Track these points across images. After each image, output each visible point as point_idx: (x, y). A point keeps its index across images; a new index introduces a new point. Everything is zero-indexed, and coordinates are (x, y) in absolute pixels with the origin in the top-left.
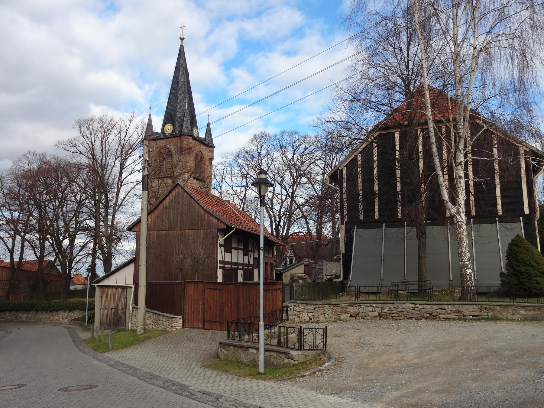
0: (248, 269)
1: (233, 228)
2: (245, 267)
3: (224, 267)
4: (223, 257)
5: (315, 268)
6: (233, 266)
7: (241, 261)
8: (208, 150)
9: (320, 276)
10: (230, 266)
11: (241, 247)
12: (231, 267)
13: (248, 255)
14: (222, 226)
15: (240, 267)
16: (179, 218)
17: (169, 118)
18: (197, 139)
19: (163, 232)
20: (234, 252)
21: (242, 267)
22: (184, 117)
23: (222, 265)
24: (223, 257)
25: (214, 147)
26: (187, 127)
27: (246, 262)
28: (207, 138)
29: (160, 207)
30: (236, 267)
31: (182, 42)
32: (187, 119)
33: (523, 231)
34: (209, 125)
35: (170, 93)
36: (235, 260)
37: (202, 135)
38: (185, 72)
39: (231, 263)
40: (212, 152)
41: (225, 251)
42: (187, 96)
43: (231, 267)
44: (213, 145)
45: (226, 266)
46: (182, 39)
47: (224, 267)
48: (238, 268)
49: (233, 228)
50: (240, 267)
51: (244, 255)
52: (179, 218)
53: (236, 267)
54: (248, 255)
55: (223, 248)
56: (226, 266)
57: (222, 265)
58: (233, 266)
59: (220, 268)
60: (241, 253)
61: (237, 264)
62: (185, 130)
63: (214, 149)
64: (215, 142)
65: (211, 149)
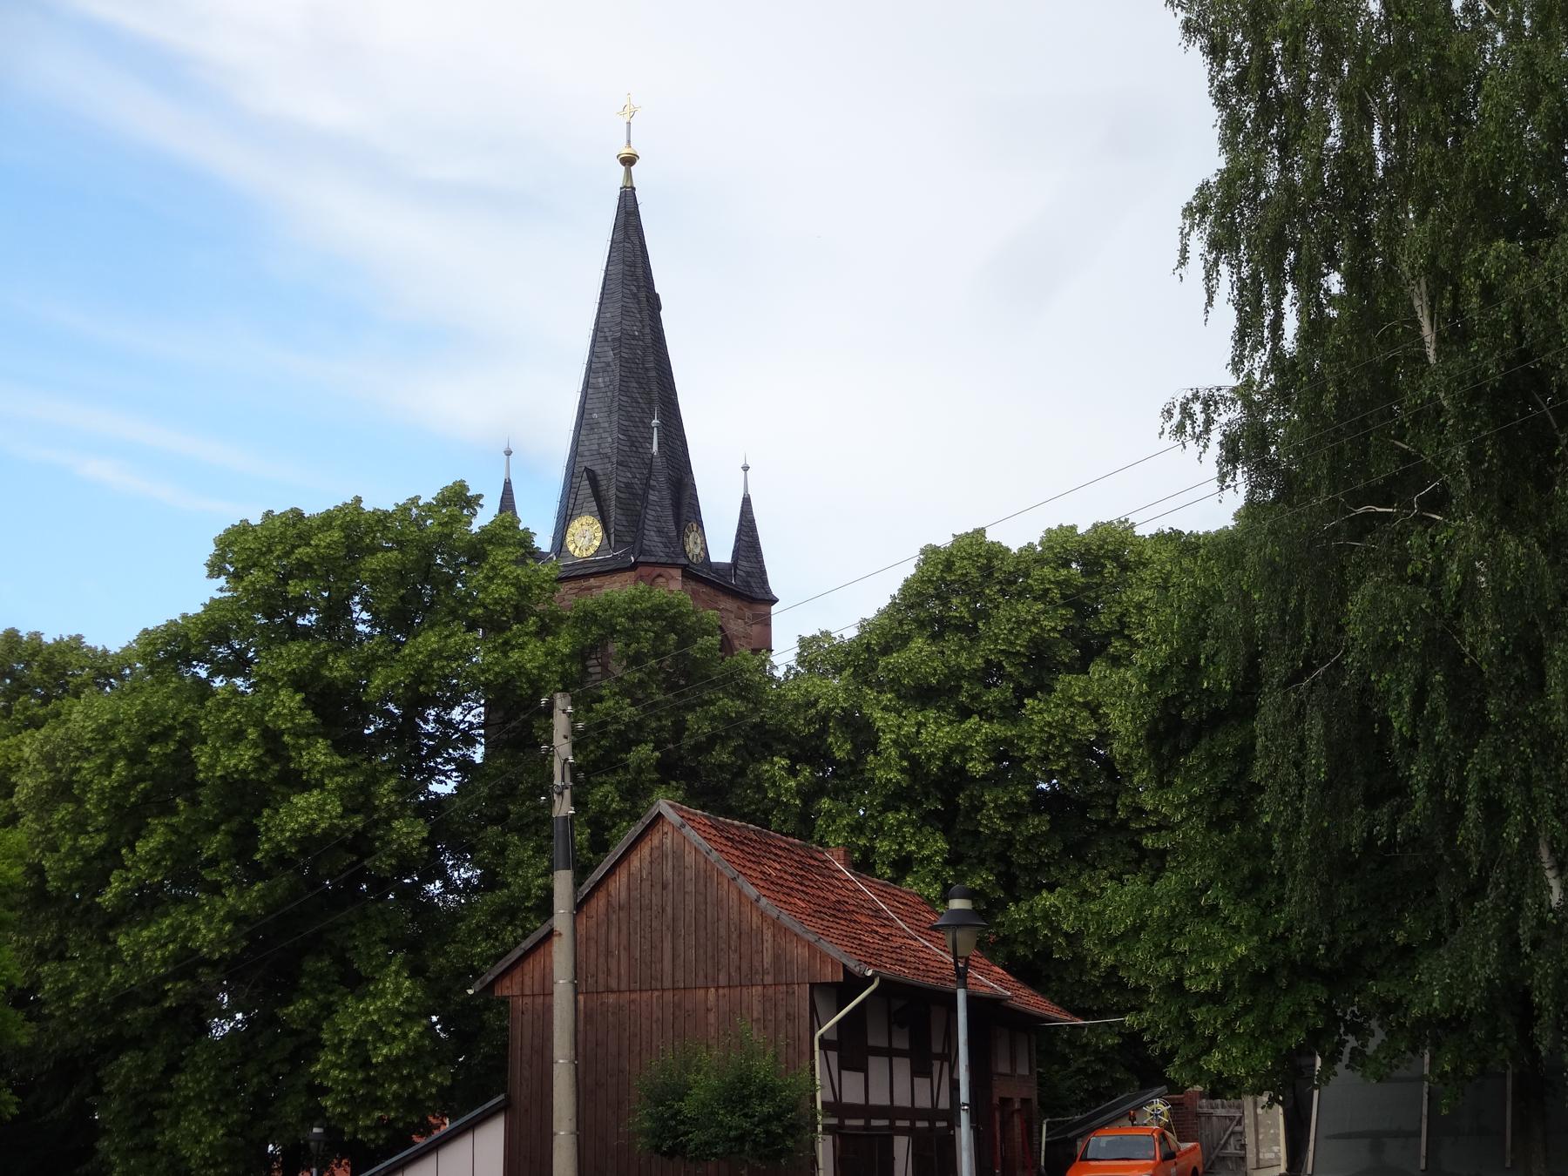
0: (932, 1128)
1: (870, 980)
2: (919, 1124)
3: (841, 1126)
4: (837, 1092)
5: (1209, 1116)
6: (875, 1123)
7: (902, 1100)
8: (748, 613)
9: (1231, 1150)
10: (861, 1122)
11: (902, 1043)
12: (867, 1127)
13: (929, 1074)
14: (830, 975)
15: (899, 1123)
16: (668, 945)
17: (585, 486)
18: (702, 575)
19: (612, 998)
20: (877, 1066)
21: (906, 1123)
22: (647, 486)
23: (834, 1121)
24: (837, 1092)
25: (774, 601)
26: (660, 531)
27: (923, 1101)
28: (743, 563)
29: (593, 902)
30: (885, 1123)
31: (629, 175)
32: (659, 496)
33: (964, 1096)
34: (746, 501)
35: (587, 384)
36: (879, 1098)
37: (721, 549)
38: (642, 295)
39: (867, 1111)
40: (766, 623)
41: (841, 1067)
42: (655, 396)
43: (867, 1127)
44: (768, 592)
45: (848, 1122)
46: (629, 161)
47: (841, 1126)
48: (892, 1127)
49: (870, 980)
50: (899, 1123)
51: (915, 1073)
52: (668, 945)
53: (885, 1123)
54: (929, 1074)
55: (833, 1056)
56: (848, 1122)
57: (834, 1121)
58: (875, 1123)
59: (827, 1129)
60: (903, 1067)
61: (890, 1112)
62: (652, 539)
63: (774, 609)
64: (777, 581)
65: (761, 609)
